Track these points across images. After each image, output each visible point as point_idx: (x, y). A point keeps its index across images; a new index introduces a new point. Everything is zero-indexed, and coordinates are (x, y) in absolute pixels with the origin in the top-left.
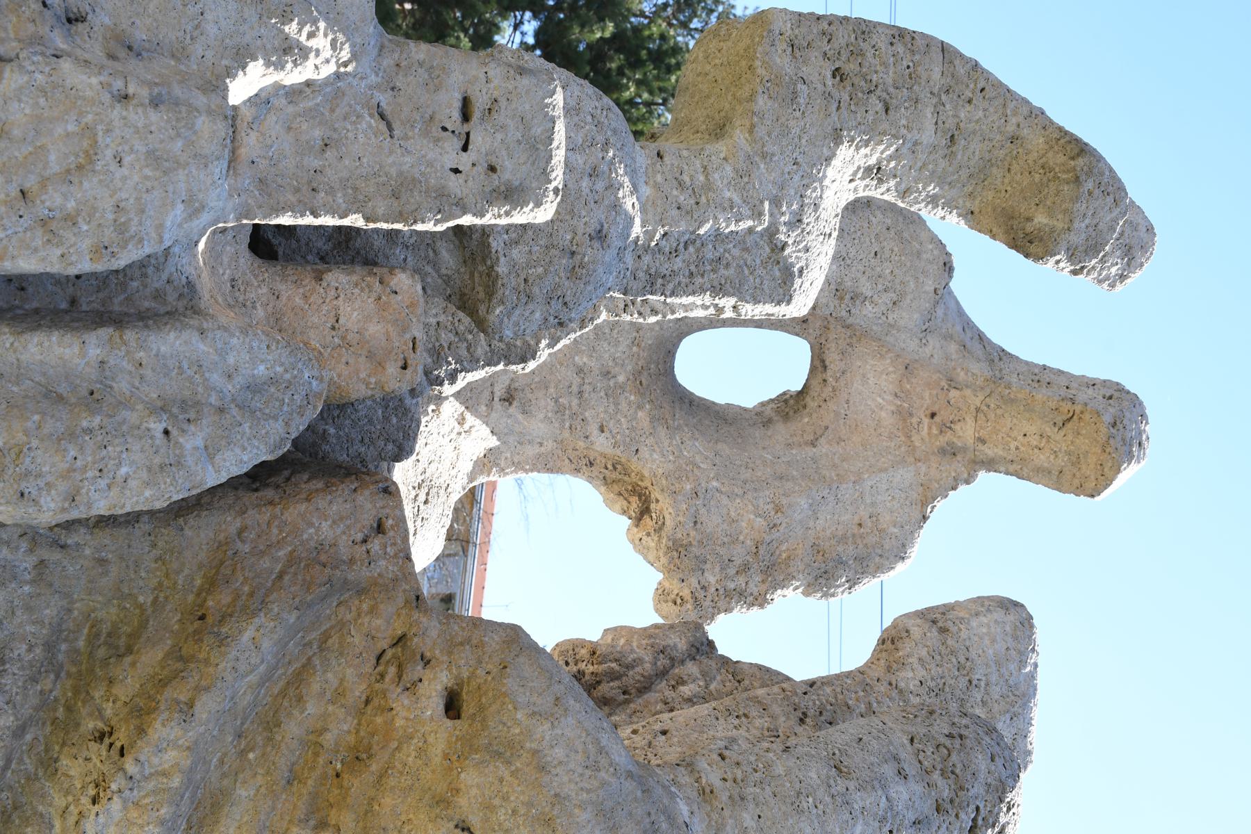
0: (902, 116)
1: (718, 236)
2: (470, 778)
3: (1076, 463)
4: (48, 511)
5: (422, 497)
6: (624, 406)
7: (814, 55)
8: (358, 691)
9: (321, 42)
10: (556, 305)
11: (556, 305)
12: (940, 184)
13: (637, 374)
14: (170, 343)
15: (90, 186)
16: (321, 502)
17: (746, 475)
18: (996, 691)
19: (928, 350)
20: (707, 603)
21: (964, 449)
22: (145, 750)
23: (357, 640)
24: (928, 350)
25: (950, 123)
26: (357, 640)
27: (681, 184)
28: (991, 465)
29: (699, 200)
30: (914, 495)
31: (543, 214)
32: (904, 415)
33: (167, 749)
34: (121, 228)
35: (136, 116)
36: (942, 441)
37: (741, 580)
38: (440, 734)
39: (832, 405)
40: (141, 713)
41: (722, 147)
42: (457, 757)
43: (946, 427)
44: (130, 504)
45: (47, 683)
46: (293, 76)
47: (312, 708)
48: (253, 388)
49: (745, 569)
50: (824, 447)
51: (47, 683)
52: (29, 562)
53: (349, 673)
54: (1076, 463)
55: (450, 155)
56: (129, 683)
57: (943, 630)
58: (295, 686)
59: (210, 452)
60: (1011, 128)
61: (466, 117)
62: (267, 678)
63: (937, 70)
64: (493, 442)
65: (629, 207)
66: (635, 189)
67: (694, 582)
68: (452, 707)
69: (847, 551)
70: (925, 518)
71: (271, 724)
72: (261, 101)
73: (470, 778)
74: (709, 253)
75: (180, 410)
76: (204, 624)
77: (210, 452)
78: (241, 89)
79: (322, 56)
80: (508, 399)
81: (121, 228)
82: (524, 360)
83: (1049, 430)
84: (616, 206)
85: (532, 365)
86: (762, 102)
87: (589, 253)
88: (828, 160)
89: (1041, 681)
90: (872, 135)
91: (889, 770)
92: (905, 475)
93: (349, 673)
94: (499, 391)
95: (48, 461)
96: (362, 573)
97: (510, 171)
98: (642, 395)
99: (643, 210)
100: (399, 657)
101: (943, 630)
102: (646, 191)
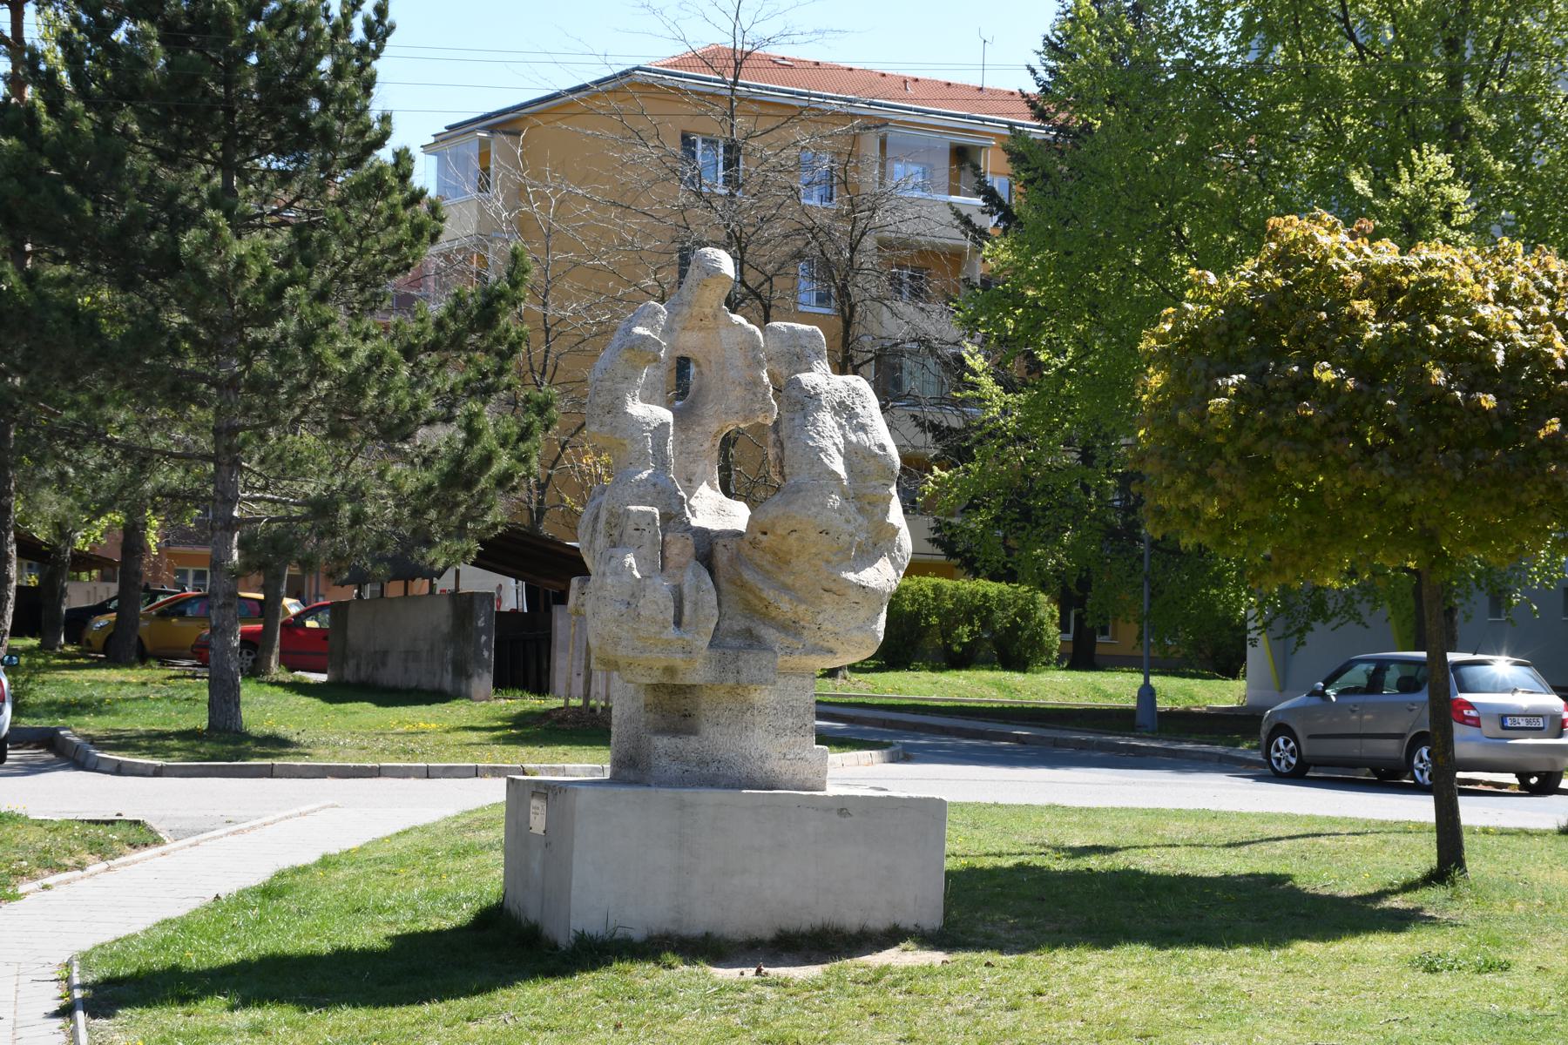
4: (716, 612)
14: (686, 590)
31: (656, 511)
32: (701, 329)
33: (769, 594)
38: (770, 537)
40: (761, 599)
53: (757, 555)
55: (646, 533)
69: (751, 354)
75: (698, 589)
79: (630, 559)
80: (690, 481)
90: (624, 402)
92: (723, 333)
93: (757, 555)
100: (754, 544)
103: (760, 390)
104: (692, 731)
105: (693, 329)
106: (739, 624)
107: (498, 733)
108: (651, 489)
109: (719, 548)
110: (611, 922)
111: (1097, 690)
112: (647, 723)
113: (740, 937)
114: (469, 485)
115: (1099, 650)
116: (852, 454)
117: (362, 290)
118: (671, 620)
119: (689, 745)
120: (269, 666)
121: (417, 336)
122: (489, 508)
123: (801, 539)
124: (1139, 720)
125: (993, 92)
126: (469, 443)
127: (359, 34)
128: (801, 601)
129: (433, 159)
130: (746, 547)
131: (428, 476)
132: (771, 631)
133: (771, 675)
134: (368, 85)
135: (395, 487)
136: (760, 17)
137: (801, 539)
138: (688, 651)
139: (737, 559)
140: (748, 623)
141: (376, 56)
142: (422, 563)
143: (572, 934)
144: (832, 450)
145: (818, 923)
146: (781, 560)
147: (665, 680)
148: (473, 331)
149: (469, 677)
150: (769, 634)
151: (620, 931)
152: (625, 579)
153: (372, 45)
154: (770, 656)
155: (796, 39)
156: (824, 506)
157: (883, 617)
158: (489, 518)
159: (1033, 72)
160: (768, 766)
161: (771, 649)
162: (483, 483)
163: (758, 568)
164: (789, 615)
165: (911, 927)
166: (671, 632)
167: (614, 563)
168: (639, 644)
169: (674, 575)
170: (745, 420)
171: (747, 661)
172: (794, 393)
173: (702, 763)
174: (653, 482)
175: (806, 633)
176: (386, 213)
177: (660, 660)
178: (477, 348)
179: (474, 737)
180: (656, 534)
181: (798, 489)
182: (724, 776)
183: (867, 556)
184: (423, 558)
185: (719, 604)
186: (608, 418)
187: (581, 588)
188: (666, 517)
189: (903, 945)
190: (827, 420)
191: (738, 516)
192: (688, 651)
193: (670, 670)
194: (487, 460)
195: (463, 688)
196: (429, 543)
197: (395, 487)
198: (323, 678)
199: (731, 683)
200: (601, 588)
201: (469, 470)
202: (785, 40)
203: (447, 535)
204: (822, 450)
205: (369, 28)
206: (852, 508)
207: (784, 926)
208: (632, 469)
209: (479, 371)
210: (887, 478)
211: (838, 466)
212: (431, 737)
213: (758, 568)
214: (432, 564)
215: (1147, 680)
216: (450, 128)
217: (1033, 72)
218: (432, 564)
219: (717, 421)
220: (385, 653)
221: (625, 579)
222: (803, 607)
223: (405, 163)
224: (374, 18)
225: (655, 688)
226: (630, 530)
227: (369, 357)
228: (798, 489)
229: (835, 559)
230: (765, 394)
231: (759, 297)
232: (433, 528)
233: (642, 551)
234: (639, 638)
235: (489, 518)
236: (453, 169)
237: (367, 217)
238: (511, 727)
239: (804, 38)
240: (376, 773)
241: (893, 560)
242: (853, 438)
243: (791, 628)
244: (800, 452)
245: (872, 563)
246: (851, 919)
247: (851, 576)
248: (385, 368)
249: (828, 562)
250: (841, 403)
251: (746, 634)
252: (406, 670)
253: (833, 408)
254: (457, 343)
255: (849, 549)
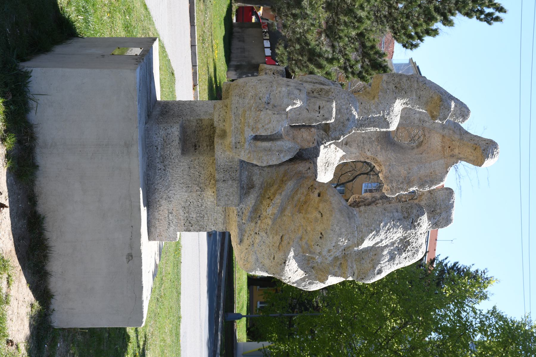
0: (409, 94)
1: (373, 118)
2: (321, 205)
3: (477, 159)
4: (264, 164)
5: (327, 165)
6: (374, 145)
7: (391, 84)
8: (306, 193)
9: (299, 102)
10: (341, 131)
11: (341, 131)
12: (419, 105)
13: (377, 138)
14: (279, 143)
15: (270, 125)
16: (300, 164)
17: (403, 161)
18: (443, 206)
19: (445, 132)
20: (394, 191)
21: (456, 155)
22: (275, 199)
23: (305, 185)
24: (445, 132)
25: (419, 95)
26: (305, 185)
27: (365, 109)
28: (461, 159)
29: (369, 111)
30: (444, 166)
32: (443, 147)
33: (278, 199)
34: (274, 129)
35: (275, 116)
36: (451, 153)
37: (402, 186)
38: (317, 199)
39: (427, 145)
40: (274, 194)
41: (373, 102)
42: (318, 202)
43: (452, 150)
44: (274, 163)
45: (261, 190)
46: (295, 107)
47: (299, 195)
48: (289, 148)
49: (402, 183)
50: (424, 155)
51: (261, 190)
52: (259, 172)
53: (304, 190)
54: (477, 159)
55: (317, 114)
56: (272, 191)
57: (431, 194)
58: (296, 192)
59: (284, 157)
60: (431, 95)
61: (319, 108)
62: (292, 191)
63: (416, 85)
64: (344, 153)
65: (354, 113)
66: (356, 110)
67: (390, 186)
68: (319, 195)
69: (428, 179)
70: (448, 172)
71: (293, 198)
72: (291, 110)
73: (321, 205)
74: (372, 120)
75: (280, 151)
76: (283, 181)
77: (284, 157)
78: (288, 110)
80: (346, 144)
81: (274, 129)
82: (338, 140)
83: (473, 151)
84: (352, 114)
85: (340, 141)
86: (380, 93)
87: (346, 123)
88: (394, 103)
89: (455, 205)
90: (403, 97)
91: (394, 211)
92: (442, 161)
93: (304, 190)
94: (344, 142)
95: (265, 158)
96: (306, 175)
97: (326, 116)
98: (378, 143)
99: (358, 114)
101: (431, 194)
102: (358, 110)
103: (405, 186)
104: (184, 151)
105: (443, 142)
106: (257, 180)
107: (213, 79)
108: (346, 117)
109: (307, 165)
110: (41, 98)
111: (241, 290)
112: (189, 121)
113: (36, 190)
114: (310, 60)
115: (255, 287)
116: (375, 253)
117: (385, 16)
118: (258, 133)
119: (175, 149)
120: (238, 2)
121: (368, 38)
122: (301, 70)
123: (316, 220)
124: (230, 314)
125: (435, 244)
126: (327, 59)
127: (487, 10)
128: (274, 221)
129: (407, 62)
130: (309, 183)
131: (313, 43)
132: (253, 201)
133: (223, 203)
134: (468, 15)
135: (308, 31)
136: (466, 167)
137: (316, 220)
138: (237, 146)
139: (301, 177)
140: (258, 186)
141: (478, 18)
142: (278, 44)
143: (29, 69)
144: (377, 239)
145: (51, 243)
146: (302, 207)
147: (217, 131)
148: (370, 61)
149: (236, 70)
150: (251, 200)
151: (35, 104)
152: (285, 101)
153: (483, 16)
154: (236, 201)
155: (458, 180)
156: (340, 235)
157: (266, 274)
158: (297, 70)
159: (446, 259)
160: (163, 202)
161: (241, 201)
162: (311, 66)
163: (295, 191)
164: (264, 213)
165: (52, 307)
166: (249, 133)
167: (296, 92)
168: (240, 111)
169: (288, 135)
170: (386, 178)
171: (232, 186)
172: (415, 211)
173: (163, 159)
174: (350, 118)
175: (253, 224)
176: (418, 23)
177: (230, 127)
178: (363, 63)
179: (212, 70)
180: (316, 121)
181: (350, 217)
182: (155, 173)
183: (306, 264)
184: (280, 44)
185: (270, 166)
186: (392, 86)
187: (278, 72)
188: (326, 128)
189: (36, 304)
190: (397, 234)
191: (325, 176)
192: (237, 146)
193: (224, 135)
194: (320, 67)
195: (232, 69)
196: (285, 47)
197: (308, 31)
198: (234, 21)
199: (217, 177)
200: (279, 84)
201: (316, 60)
202: (458, 176)
203: (289, 53)
204: (378, 232)
205: (490, 14)
206: (338, 254)
207: (47, 220)
208: (358, 104)
209: (353, 65)
210: (359, 275)
211: (367, 243)
212: (211, 53)
213: (295, 191)
214: (278, 48)
215: (244, 316)
216: (418, 67)
217: (446, 259)
218: (278, 48)
219: (383, 161)
220: (244, 41)
221: (285, 101)
222: (270, 223)
223: (433, 33)
224: (494, 16)
225: (212, 127)
226: (319, 103)
227: (361, 17)
228: (350, 217)
229: (303, 243)
230: (402, 189)
231: (371, 171)
232: (292, 48)
233: (305, 112)
234: (245, 111)
235: (297, 70)
236: (406, 68)
237: (416, 15)
238: (216, 85)
239: (458, 182)
240: (192, 25)
241: (303, 280)
242: (385, 252)
243: (256, 214)
244: (376, 217)
245: (301, 266)
246: (55, 266)
247: (292, 254)
248: (356, 24)
249: (301, 238)
250: (408, 243)
251: (249, 183)
252: (237, 49)
253: (405, 238)
254: (365, 55)
255: (310, 252)
